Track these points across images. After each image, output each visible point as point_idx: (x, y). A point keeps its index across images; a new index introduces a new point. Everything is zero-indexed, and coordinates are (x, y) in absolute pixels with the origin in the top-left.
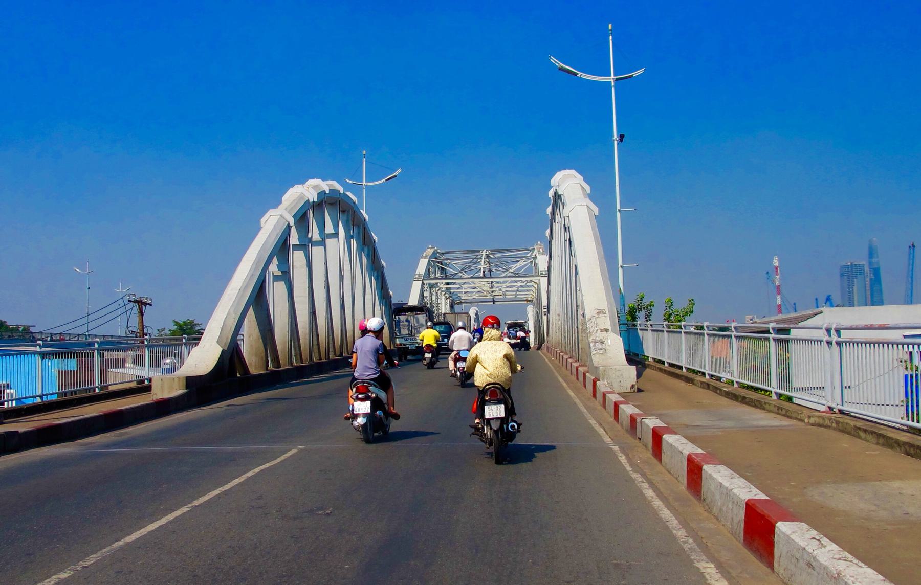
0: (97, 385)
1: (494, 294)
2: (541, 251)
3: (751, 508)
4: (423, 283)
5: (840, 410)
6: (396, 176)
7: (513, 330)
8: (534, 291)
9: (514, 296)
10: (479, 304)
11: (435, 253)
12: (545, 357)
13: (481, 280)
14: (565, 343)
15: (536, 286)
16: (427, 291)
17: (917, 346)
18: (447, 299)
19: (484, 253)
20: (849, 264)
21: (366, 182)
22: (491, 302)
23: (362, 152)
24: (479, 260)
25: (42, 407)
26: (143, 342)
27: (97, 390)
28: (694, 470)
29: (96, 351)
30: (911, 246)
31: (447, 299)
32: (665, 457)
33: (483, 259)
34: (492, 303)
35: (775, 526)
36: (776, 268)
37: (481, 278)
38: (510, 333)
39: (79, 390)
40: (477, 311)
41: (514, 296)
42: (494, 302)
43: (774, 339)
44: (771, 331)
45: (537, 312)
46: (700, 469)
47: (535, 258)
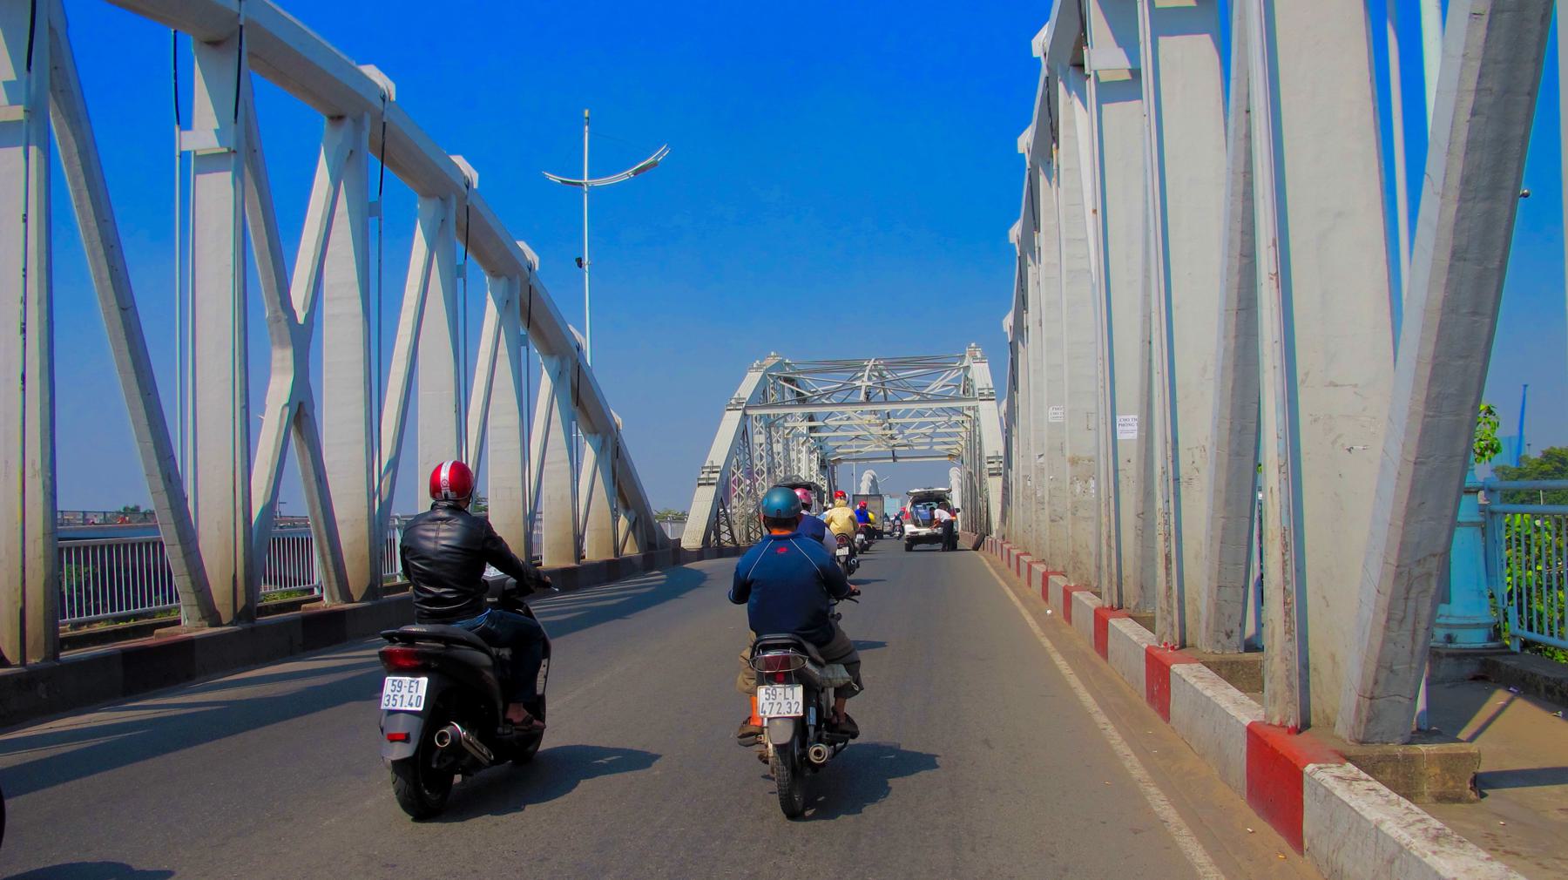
1: (893, 442)
2: (979, 356)
3: (1256, 737)
4: (745, 415)
5: (1526, 644)
6: (654, 164)
7: (925, 507)
8: (964, 435)
9: (927, 447)
11: (780, 366)
12: (1002, 582)
13: (860, 408)
14: (1169, 588)
15: (967, 425)
16: (761, 433)
17: (1519, 515)
18: (811, 452)
19: (871, 363)
22: (890, 458)
23: (583, 113)
24: (860, 374)
28: (1158, 671)
31: (811, 452)
32: (1177, 707)
33: (867, 371)
34: (892, 461)
35: (1302, 772)
37: (861, 403)
38: (917, 513)
40: (874, 477)
41: (927, 447)
42: (895, 458)
45: (970, 473)
46: (1106, 623)
47: (967, 368)
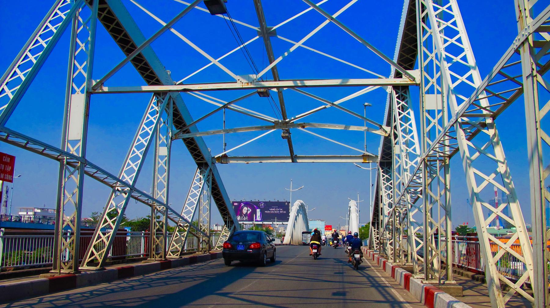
0: (142, 253)
10: (264, 161)
20: (493, 199)
21: (292, 190)
25: (32, 272)
26: (142, 234)
27: (185, 251)
29: (142, 237)
30: (548, 187)
34: (290, 161)
36: (496, 192)
39: (131, 256)
43: (457, 242)
44: (456, 238)
